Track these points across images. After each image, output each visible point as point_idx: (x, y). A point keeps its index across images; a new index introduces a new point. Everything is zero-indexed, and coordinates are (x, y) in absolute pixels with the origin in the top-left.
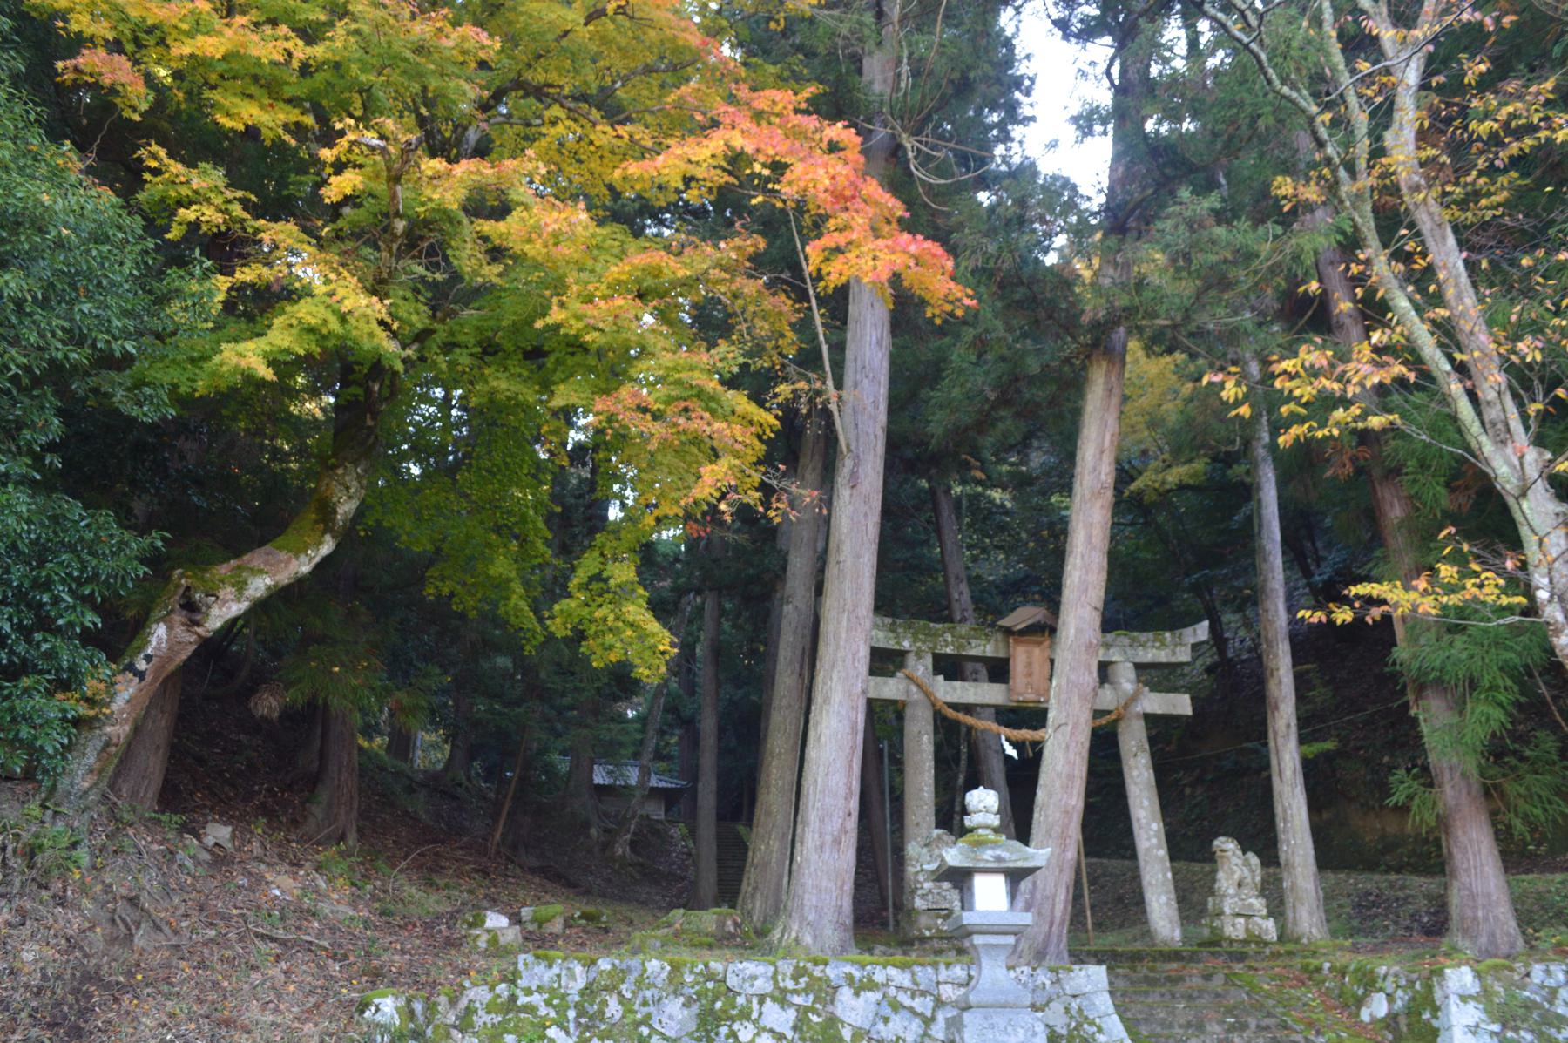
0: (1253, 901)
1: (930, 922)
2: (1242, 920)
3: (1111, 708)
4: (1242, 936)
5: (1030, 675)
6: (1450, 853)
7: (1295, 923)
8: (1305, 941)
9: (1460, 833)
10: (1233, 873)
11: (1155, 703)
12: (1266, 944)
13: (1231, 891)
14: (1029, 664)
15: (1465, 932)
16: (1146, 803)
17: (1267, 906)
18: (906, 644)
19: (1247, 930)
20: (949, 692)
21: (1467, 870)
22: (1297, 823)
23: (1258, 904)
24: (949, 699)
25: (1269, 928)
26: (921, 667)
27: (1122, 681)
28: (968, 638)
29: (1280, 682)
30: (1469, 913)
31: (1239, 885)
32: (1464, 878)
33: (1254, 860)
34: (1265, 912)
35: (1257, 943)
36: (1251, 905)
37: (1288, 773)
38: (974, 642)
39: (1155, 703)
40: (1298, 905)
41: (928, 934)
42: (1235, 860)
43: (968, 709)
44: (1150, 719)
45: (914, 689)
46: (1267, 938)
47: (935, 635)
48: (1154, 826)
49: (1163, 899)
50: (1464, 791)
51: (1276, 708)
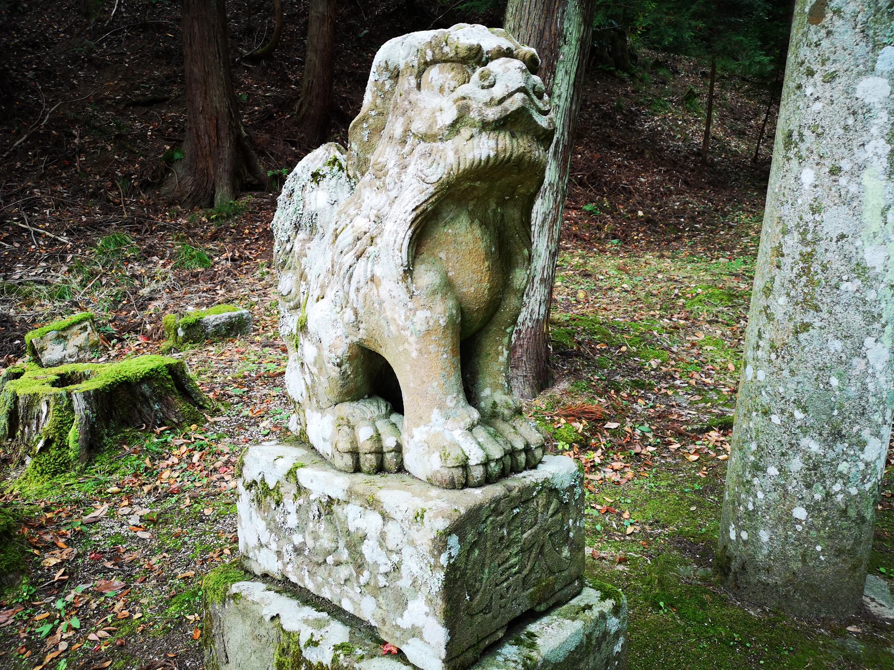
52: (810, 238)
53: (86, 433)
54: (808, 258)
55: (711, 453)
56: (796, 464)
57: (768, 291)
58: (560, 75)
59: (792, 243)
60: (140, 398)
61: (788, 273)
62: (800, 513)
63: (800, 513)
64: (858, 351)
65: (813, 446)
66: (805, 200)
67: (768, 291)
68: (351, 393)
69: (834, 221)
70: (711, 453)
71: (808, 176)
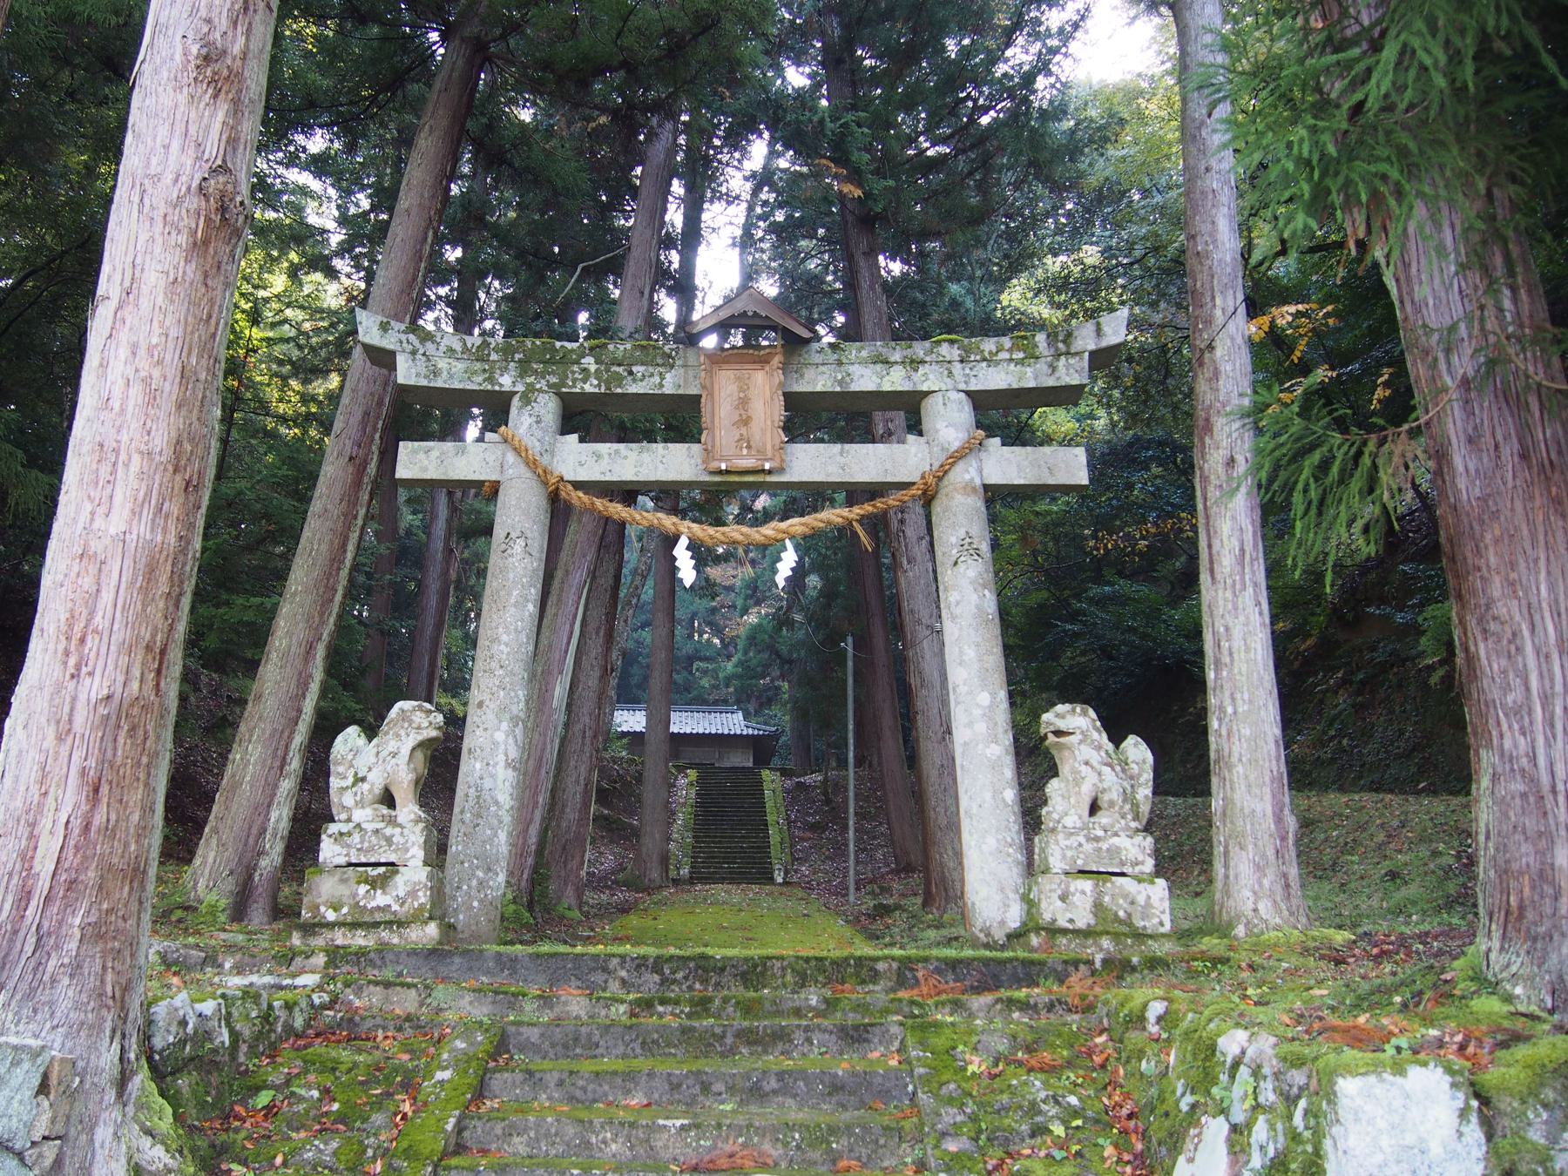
0: (1122, 841)
1: (343, 891)
2: (1087, 885)
3: (915, 477)
4: (1084, 919)
5: (746, 422)
6: (1471, 659)
7: (1227, 893)
8: (1240, 931)
9: (1496, 588)
10: (1078, 781)
11: (1006, 465)
12: (1140, 936)
13: (1071, 821)
14: (744, 403)
15: (1513, 920)
16: (970, 653)
17: (1157, 853)
18: (506, 381)
19: (1098, 907)
20: (581, 460)
21: (1521, 711)
22: (1241, 666)
23: (1137, 849)
24: (583, 476)
25: (1154, 902)
26: (533, 420)
27: (940, 425)
28: (627, 362)
29: (1216, 375)
30: (1525, 855)
31: (1094, 808)
32: (1512, 740)
33: (1137, 750)
34: (1149, 865)
35: (1116, 936)
36: (1114, 852)
37: (1226, 562)
38: (638, 369)
39: (1006, 465)
40: (1234, 850)
41: (331, 916)
42: (1086, 752)
43: (627, 493)
44: (995, 496)
45: (511, 457)
46: (1150, 925)
47: (566, 360)
48: (984, 698)
49: (991, 842)
50: (1509, 451)
51: (1208, 428)
52: (479, 789)
53: (1190, 394)
54: (478, 797)
55: (809, 779)
56: (474, 883)
57: (462, 812)
58: (308, 700)
59: (472, 791)
60: (1381, 422)
61: (471, 803)
62: (475, 904)
63: (475, 904)
64: (496, 835)
65: (480, 874)
66: (477, 775)
67: (462, 812)
68: (382, 803)
69: (487, 784)
70: (809, 779)
71: (478, 766)
